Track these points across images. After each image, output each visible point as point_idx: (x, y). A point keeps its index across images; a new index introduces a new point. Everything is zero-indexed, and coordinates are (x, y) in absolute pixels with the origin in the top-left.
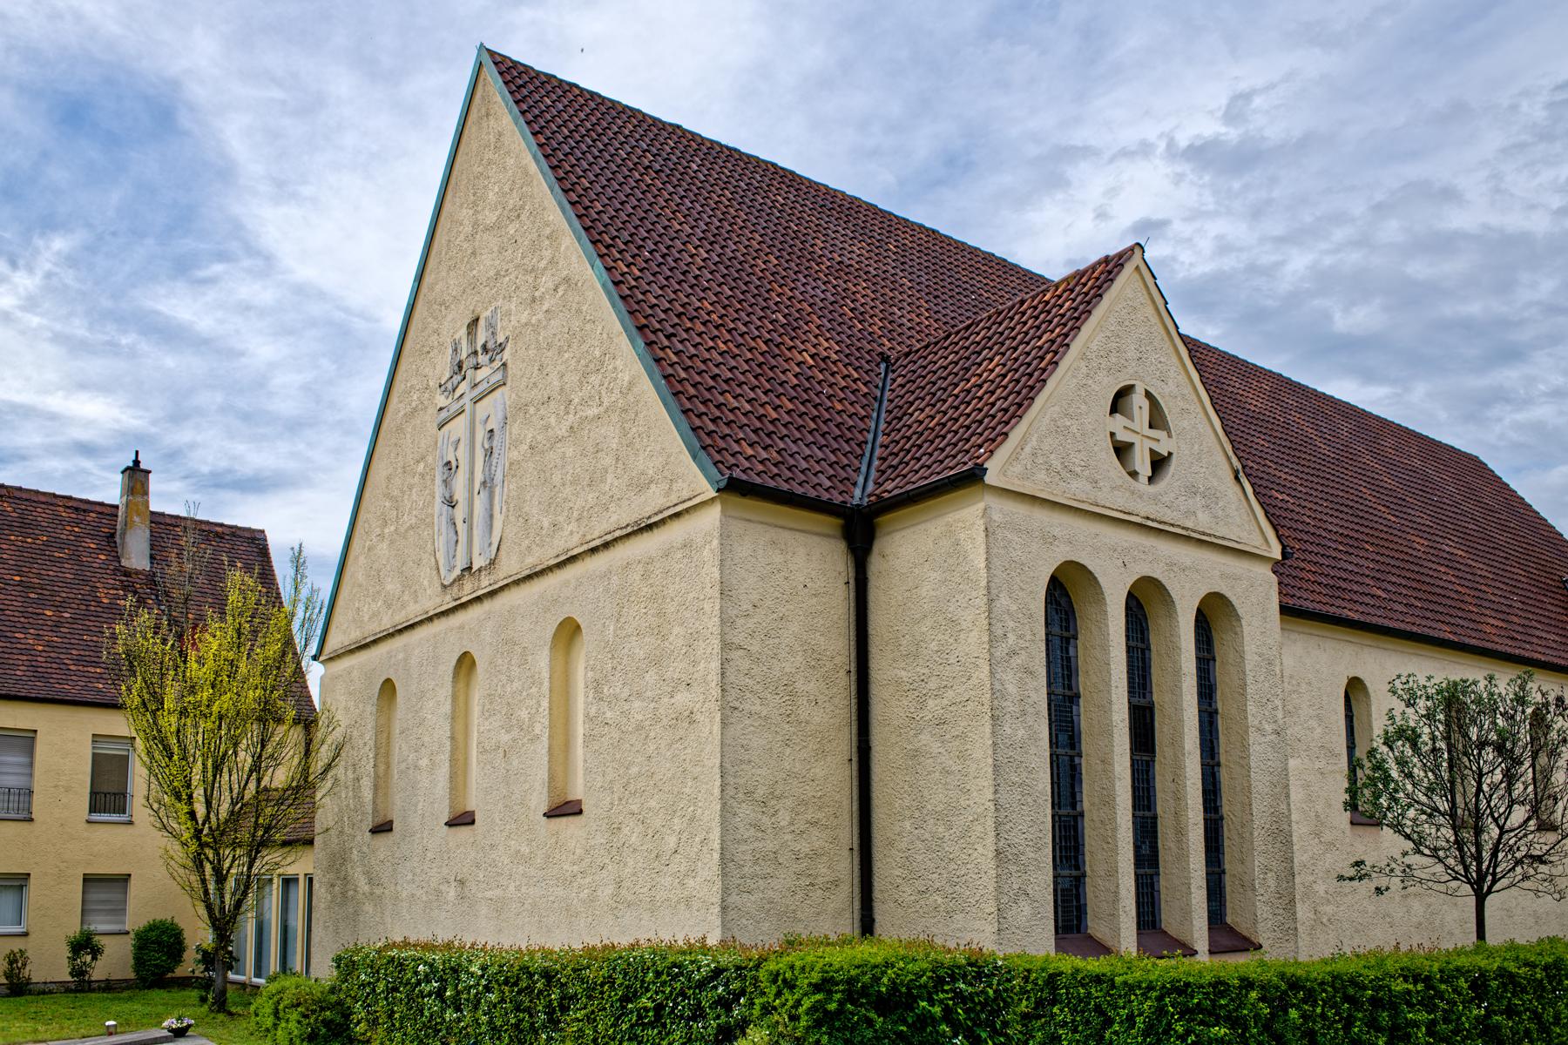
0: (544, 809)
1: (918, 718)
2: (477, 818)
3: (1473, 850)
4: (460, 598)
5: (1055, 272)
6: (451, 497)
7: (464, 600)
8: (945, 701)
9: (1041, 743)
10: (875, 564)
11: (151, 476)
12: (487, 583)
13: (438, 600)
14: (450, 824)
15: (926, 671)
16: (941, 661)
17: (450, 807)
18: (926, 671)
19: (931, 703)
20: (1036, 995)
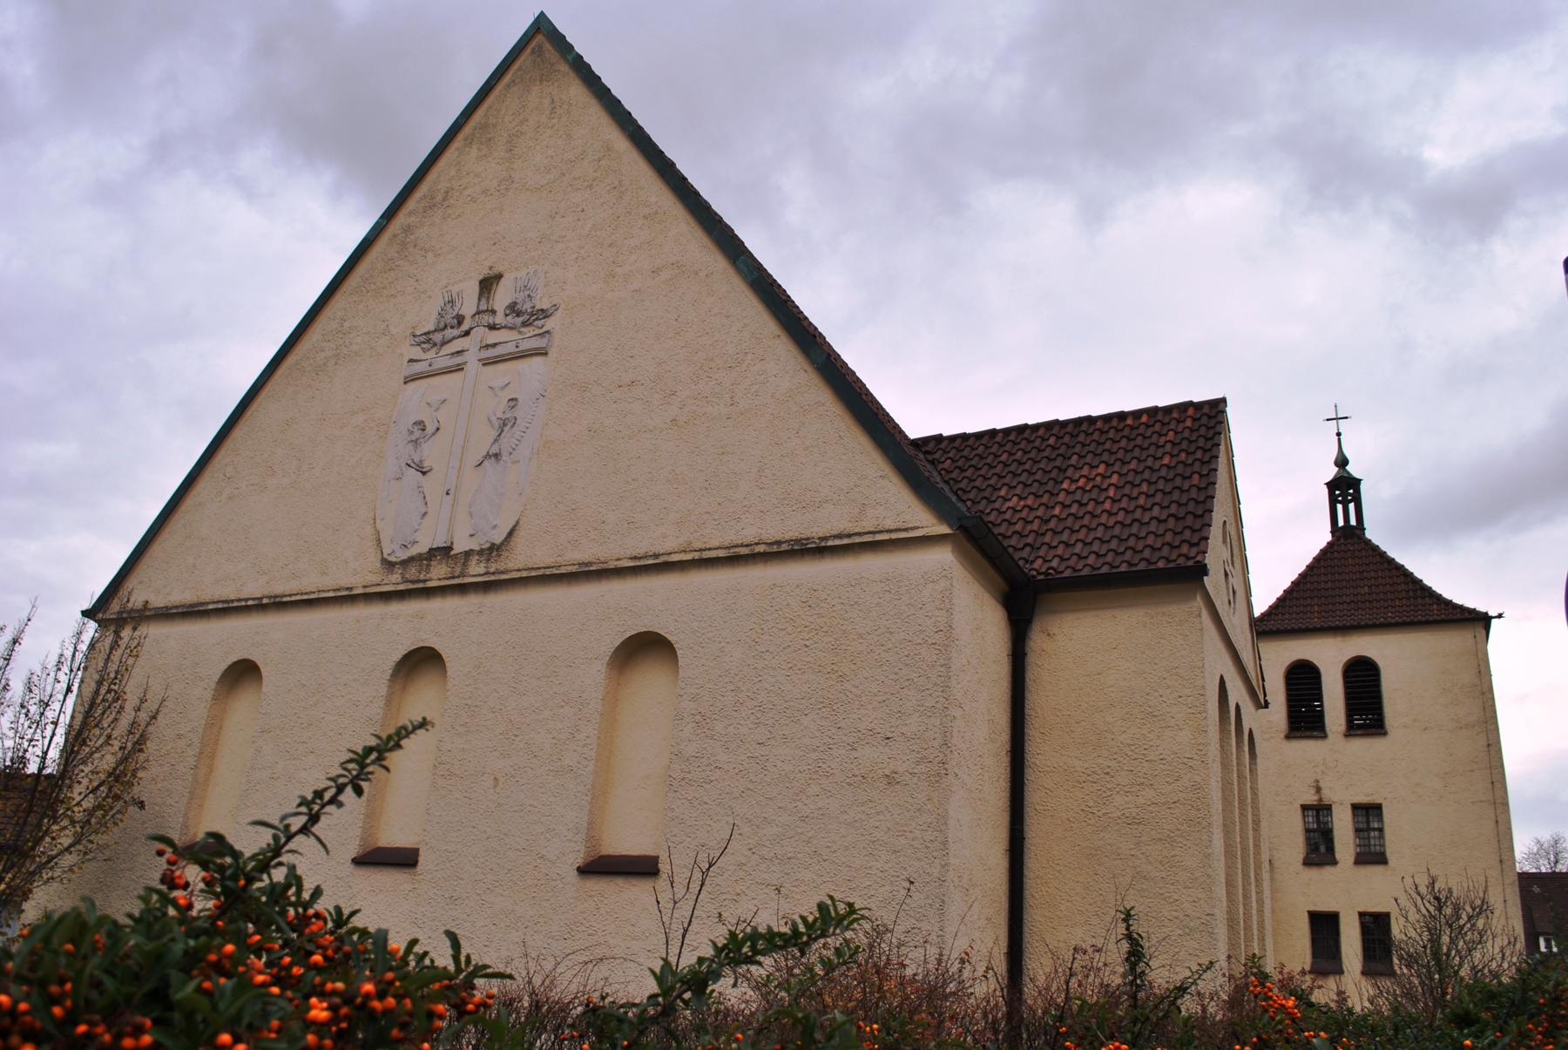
0: (580, 861)
1: (1100, 814)
2: (421, 859)
3: (775, 547)
4: (425, 581)
5: (1329, 538)
6: (421, 461)
7: (430, 584)
8: (1141, 800)
9: (224, 661)
10: (1037, 641)
12: (482, 570)
13: (375, 579)
14: (359, 862)
15: (1113, 764)
16: (1135, 756)
17: (362, 839)
18: (1113, 764)
19: (1119, 800)
20: (1401, 1021)
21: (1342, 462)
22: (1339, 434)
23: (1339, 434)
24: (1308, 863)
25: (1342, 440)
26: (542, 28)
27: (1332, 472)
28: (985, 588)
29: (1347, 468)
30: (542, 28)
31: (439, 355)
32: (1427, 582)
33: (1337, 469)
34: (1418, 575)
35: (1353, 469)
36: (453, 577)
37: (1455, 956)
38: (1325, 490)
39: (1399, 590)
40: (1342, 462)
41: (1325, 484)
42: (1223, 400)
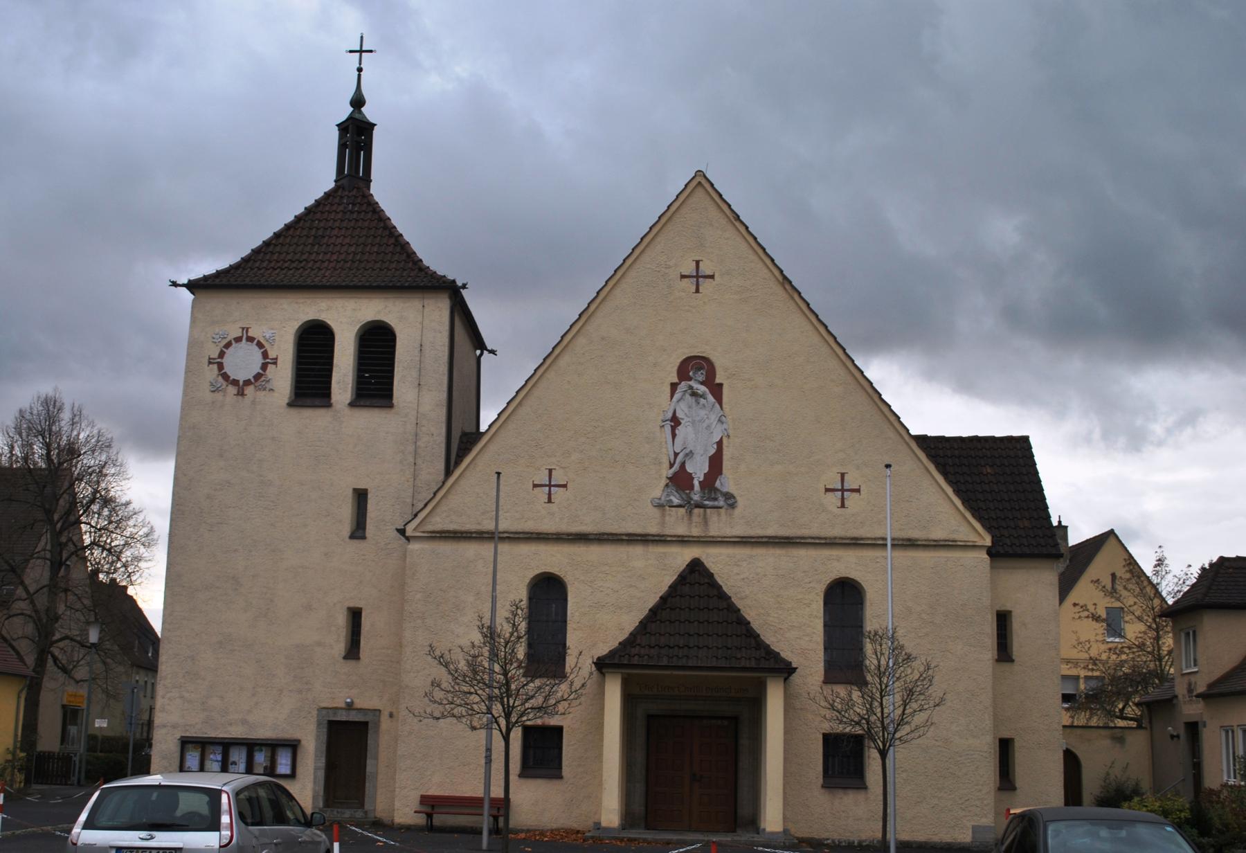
11: (375, 127)
21: (358, 102)
22: (360, 70)
23: (360, 70)
24: (346, 657)
25: (362, 76)
26: (700, 183)
27: (346, 111)
28: (1014, 748)
29: (362, 109)
30: (700, 183)
31: (1123, 606)
32: (278, 226)
33: (352, 109)
34: (289, 218)
35: (368, 112)
36: (892, 617)
37: (58, 522)
38: (335, 133)
39: (739, 656)
40: (358, 102)
41: (337, 125)
42: (375, 125)
